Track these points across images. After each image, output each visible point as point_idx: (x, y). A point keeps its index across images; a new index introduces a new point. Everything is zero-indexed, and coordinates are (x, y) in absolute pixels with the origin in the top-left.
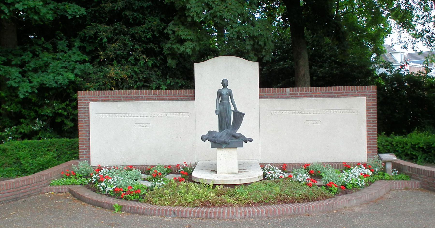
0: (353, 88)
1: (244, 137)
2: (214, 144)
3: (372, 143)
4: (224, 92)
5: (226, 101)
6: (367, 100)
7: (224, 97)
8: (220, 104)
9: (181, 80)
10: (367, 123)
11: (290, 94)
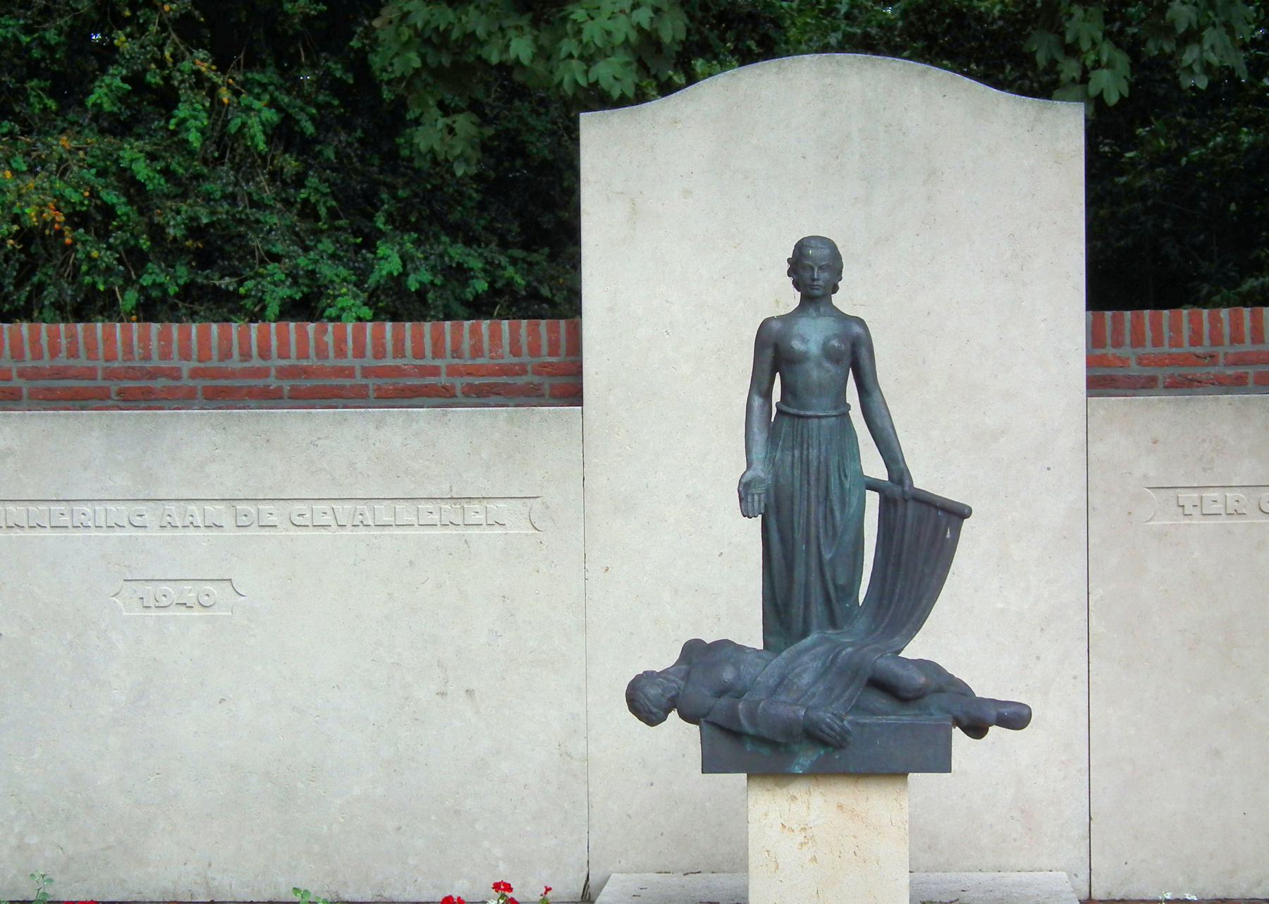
1: (962, 690)
2: (725, 745)
4: (812, 336)
5: (819, 407)
7: (809, 380)
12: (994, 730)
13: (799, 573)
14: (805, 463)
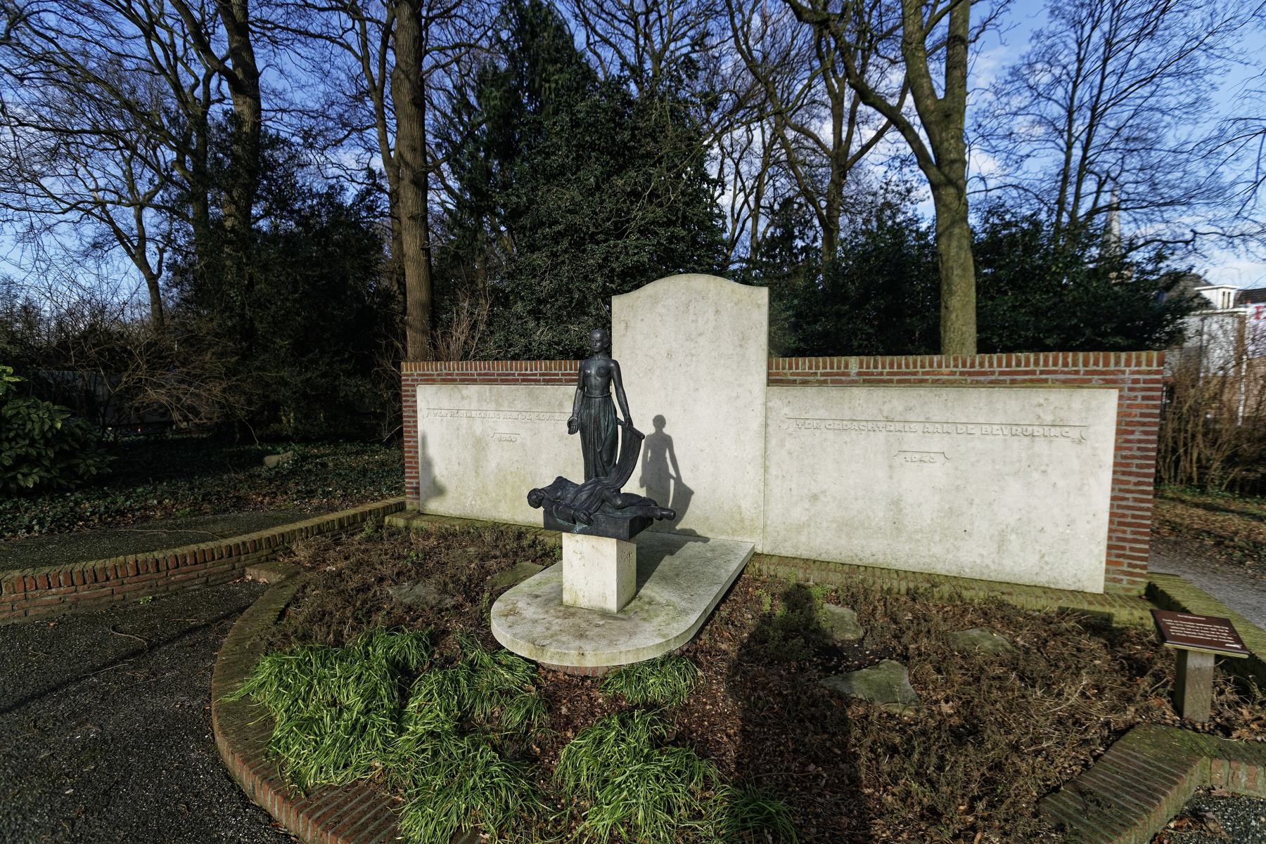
0: (1070, 360)
3: (1129, 536)
6: (1121, 397)
10: (1115, 472)
11: (859, 374)
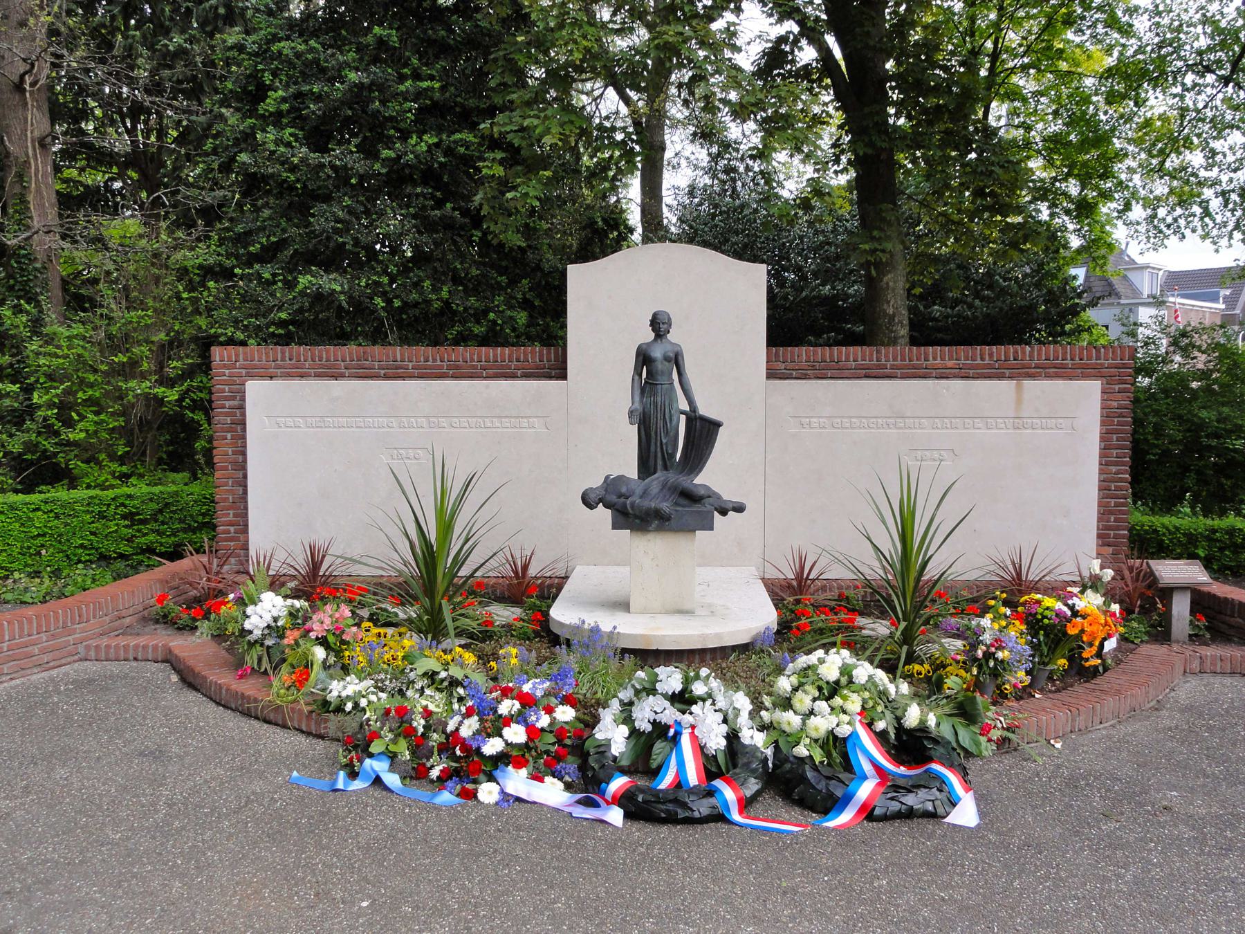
1: (719, 497)
2: (621, 519)
4: (657, 353)
5: (662, 380)
7: (654, 369)
8: (643, 390)
9: (530, 329)
12: (730, 513)
13: (653, 448)
14: (656, 404)
